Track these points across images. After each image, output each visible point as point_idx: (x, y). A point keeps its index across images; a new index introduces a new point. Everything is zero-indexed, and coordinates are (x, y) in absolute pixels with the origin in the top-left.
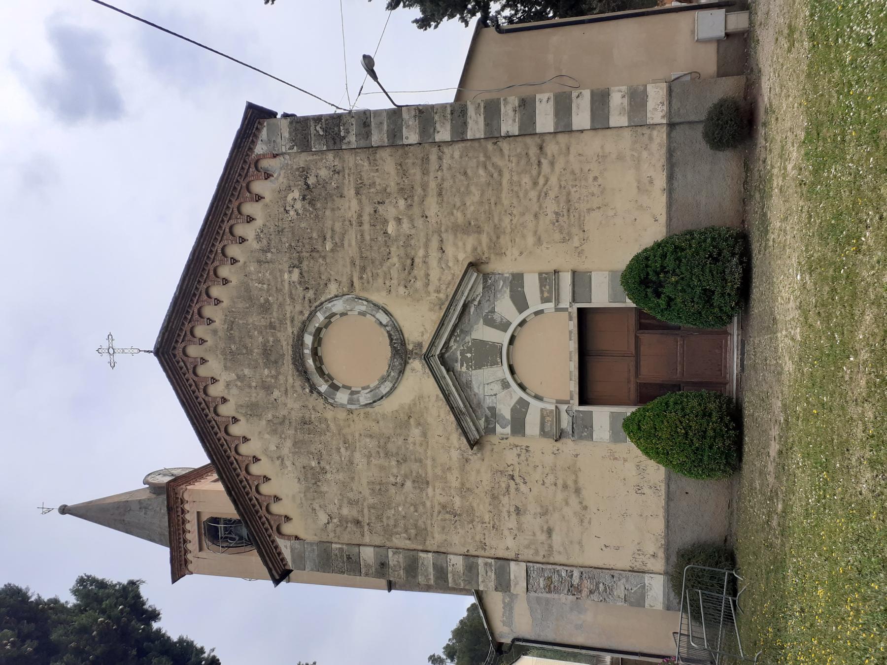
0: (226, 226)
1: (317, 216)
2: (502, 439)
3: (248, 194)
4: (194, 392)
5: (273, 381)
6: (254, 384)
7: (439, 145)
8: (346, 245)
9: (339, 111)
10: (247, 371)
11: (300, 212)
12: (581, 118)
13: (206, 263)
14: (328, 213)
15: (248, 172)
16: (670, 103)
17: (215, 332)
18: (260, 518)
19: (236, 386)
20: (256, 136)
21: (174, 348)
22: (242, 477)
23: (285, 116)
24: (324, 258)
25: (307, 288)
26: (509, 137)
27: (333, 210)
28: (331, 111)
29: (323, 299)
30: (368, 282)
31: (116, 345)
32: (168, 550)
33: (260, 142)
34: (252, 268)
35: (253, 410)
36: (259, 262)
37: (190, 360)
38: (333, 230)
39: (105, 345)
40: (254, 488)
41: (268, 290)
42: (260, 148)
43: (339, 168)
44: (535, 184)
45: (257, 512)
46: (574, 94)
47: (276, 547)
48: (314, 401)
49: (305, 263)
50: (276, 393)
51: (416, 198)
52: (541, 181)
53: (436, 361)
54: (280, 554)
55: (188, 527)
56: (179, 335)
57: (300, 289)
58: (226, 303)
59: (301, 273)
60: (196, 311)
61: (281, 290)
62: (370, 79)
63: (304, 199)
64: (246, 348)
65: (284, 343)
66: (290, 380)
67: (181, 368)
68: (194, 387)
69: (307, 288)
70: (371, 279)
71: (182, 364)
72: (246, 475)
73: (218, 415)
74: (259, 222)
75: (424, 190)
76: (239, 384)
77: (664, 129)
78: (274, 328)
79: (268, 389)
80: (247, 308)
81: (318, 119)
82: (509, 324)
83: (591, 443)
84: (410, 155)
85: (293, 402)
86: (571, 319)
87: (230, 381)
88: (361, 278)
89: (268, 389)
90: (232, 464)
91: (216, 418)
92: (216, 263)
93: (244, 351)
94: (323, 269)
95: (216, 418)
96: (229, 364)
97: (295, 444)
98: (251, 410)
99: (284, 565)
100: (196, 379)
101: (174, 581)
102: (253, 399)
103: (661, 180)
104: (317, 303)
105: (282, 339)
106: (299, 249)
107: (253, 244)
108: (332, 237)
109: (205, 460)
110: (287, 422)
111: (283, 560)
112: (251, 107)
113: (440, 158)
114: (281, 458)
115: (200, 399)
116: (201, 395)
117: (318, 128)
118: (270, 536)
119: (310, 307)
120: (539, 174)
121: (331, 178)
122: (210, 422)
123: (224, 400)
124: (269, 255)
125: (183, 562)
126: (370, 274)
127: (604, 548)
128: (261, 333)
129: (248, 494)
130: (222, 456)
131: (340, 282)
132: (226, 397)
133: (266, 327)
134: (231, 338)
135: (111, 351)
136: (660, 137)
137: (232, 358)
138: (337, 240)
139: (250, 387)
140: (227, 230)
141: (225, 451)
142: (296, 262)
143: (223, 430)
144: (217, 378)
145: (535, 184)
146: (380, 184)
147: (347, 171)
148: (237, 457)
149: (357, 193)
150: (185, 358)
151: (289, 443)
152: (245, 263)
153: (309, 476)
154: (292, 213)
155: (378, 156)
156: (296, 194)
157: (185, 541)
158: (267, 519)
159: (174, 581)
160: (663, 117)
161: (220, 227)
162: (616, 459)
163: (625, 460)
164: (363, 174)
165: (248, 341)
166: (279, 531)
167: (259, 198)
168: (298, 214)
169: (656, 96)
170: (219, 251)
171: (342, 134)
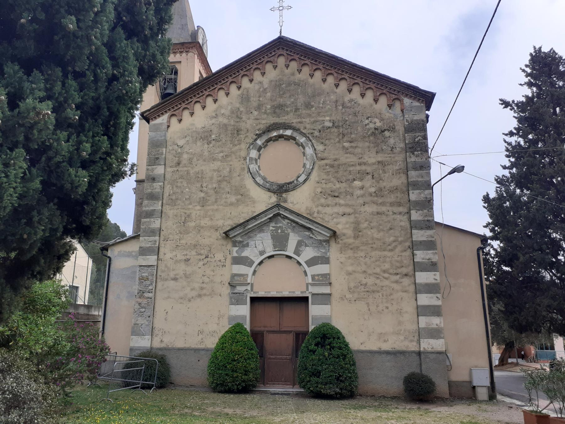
0: (358, 80)
1: (365, 137)
3: (378, 94)
4: (256, 62)
5: (263, 111)
6: (261, 99)
7: (409, 213)
8: (348, 155)
10: (269, 94)
11: (368, 127)
12: (425, 299)
13: (336, 68)
14: (367, 144)
17: (293, 74)
18: (180, 104)
19: (260, 88)
20: (415, 99)
21: (283, 49)
23: (427, 117)
24: (339, 142)
25: (320, 131)
27: (369, 147)
28: (430, 145)
29: (313, 141)
30: (324, 169)
31: (285, 11)
33: (411, 101)
34: (333, 97)
35: (245, 99)
36: (337, 101)
38: (356, 147)
40: (198, 100)
41: (319, 107)
42: (407, 101)
43: (394, 150)
44: (384, 272)
45: (184, 102)
46: (439, 295)
48: (251, 136)
49: (336, 130)
50: (256, 113)
51: (376, 198)
52: (386, 275)
54: (159, 116)
57: (320, 127)
59: (329, 127)
60: (306, 62)
63: (375, 129)
65: (286, 118)
66: (264, 122)
68: (259, 61)
69: (320, 131)
70: (326, 171)
71: (273, 54)
73: (242, 77)
74: (361, 101)
75: (381, 204)
76: (261, 90)
77: (417, 349)
81: (425, 138)
83: (228, 304)
85: (251, 123)
86: (302, 292)
87: (262, 84)
88: (326, 165)
89: (259, 107)
90: (213, 86)
92: (335, 74)
94: (332, 141)
96: (273, 83)
97: (225, 125)
102: (252, 99)
103: (386, 347)
104: (311, 138)
105: (289, 116)
108: (352, 147)
110: (238, 120)
113: (400, 213)
114: (216, 116)
115: (252, 66)
118: (169, 110)
120: (390, 274)
121: (388, 146)
123: (251, 81)
124: (341, 107)
126: (328, 170)
129: (195, 96)
130: (217, 79)
133: (296, 106)
134: (289, 84)
135: (281, 8)
136: (413, 347)
137: (277, 85)
139: (260, 97)
140: (356, 81)
142: (336, 124)
143: (233, 80)
144: (265, 76)
145: (384, 272)
147: (393, 155)
148: (217, 89)
149: (379, 162)
150: (277, 56)
151: (225, 121)
152: (336, 93)
154: (367, 122)
155: (402, 175)
156: (378, 124)
160: (424, 348)
161: (358, 77)
162: (219, 319)
163: (218, 324)
164: (391, 165)
165: (288, 95)
168: (366, 125)
169: (437, 344)
171: (416, 153)
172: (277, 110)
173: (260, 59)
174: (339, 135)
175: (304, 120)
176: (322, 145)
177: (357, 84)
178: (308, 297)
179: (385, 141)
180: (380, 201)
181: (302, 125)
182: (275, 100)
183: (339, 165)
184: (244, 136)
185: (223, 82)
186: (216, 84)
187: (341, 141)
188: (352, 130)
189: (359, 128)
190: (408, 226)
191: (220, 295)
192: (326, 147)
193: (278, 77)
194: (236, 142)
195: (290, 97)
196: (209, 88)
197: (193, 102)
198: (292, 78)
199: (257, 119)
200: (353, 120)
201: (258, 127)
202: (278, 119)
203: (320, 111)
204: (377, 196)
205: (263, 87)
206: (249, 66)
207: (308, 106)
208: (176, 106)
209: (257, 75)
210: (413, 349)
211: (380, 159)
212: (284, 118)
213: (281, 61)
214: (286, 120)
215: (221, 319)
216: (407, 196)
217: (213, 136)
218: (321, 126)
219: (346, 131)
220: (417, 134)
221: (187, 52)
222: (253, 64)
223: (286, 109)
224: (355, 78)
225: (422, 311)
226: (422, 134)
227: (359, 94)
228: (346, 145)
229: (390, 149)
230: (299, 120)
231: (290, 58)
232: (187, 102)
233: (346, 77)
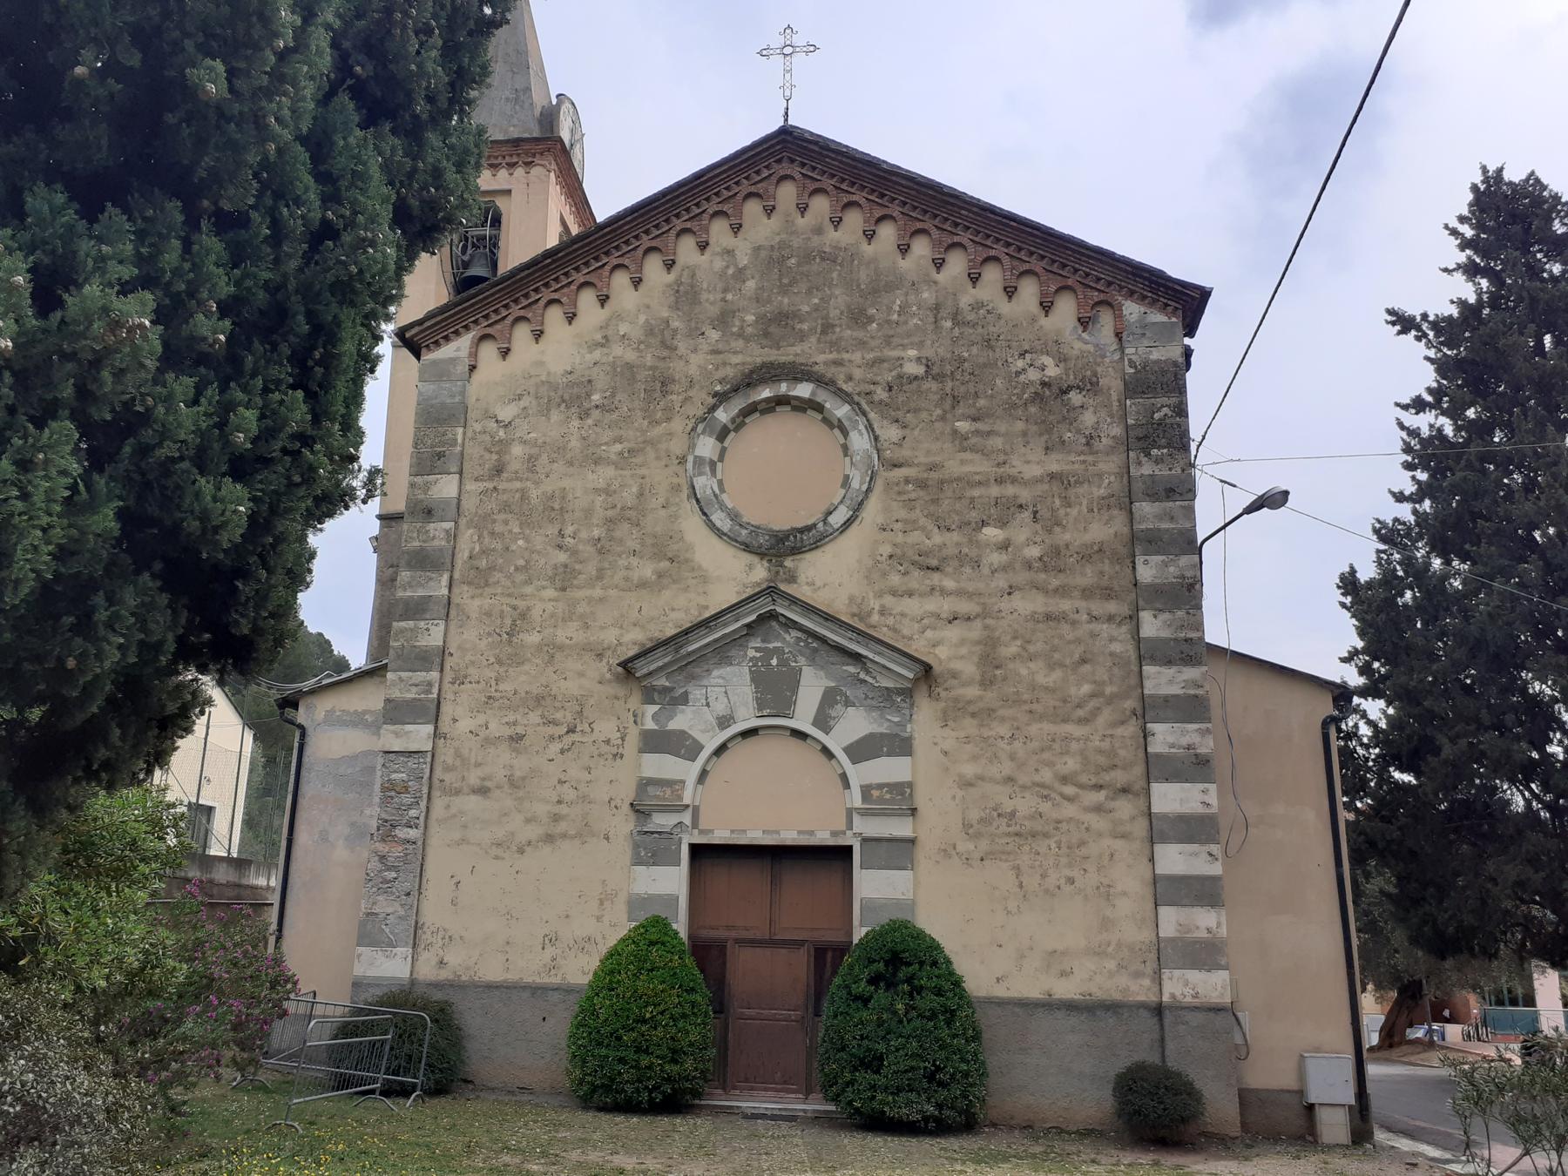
0: (999, 250)
1: (1014, 406)
3: (1053, 288)
4: (717, 194)
6: (729, 297)
7: (1134, 618)
8: (968, 456)
10: (751, 284)
11: (1022, 377)
12: (1175, 859)
13: (936, 216)
16: (1196, 1008)
17: (819, 231)
18: (506, 306)
23: (1188, 353)
25: (890, 389)
26: (1145, 737)
27: (1025, 434)
28: (1195, 432)
29: (872, 415)
30: (899, 493)
31: (799, 58)
33: (1143, 309)
35: (685, 295)
36: (937, 308)
38: (989, 433)
39: (799, 40)
41: (888, 322)
42: (1132, 310)
44: (1064, 780)
45: (516, 301)
46: (1214, 848)
49: (934, 386)
50: (714, 335)
52: (1069, 790)
59: (916, 378)
60: (854, 198)
63: (1044, 384)
65: (798, 349)
66: (736, 359)
68: (726, 194)
69: (890, 389)
70: (905, 497)
71: (765, 173)
73: (678, 235)
74: (1005, 307)
75: (1056, 590)
76: (730, 271)
77: (1154, 998)
78: (824, 332)
80: (859, 286)
81: (1181, 411)
84: (1117, 568)
85: (699, 362)
86: (834, 834)
88: (907, 481)
89: (723, 320)
90: (597, 259)
92: (935, 233)
93: (785, 281)
94: (924, 415)
96: (763, 254)
97: (629, 366)
102: (704, 296)
103: (1066, 989)
105: (805, 346)
107: (969, 295)
108: (977, 432)
110: (665, 353)
112: (1204, 295)
113: (1110, 618)
115: (705, 205)
120: (1081, 786)
121: (1078, 431)
122: (667, 221)
123: (703, 247)
124: (949, 324)
126: (913, 496)
127: (455, 880)
128: (816, 309)
130: (609, 242)
133: (826, 317)
134: (807, 257)
135: (788, 50)
136: (1140, 991)
137: (774, 259)
139: (725, 290)
140: (992, 253)
141: (617, 248)
143: (654, 244)
144: (740, 234)
145: (1064, 780)
147: (1090, 458)
148: (607, 268)
149: (1052, 476)
150: (774, 179)
151: (630, 356)
154: (1020, 364)
155: (1116, 512)
156: (1052, 371)
160: (1173, 996)
162: (602, 903)
163: (599, 919)
164: (1086, 486)
165: (803, 287)
168: (1018, 373)
169: (1210, 985)
170: (956, 239)
171: (1155, 452)
175: (846, 356)
177: (996, 259)
178: (850, 848)
179: (1070, 416)
182: (769, 301)
183: (942, 482)
186: (607, 253)
187: (949, 416)
191: (607, 839)
193: (777, 239)
198: (816, 240)
201: (720, 374)
203: (891, 332)
204: (1045, 569)
205: (736, 266)
207: (858, 318)
209: (719, 231)
211: (1055, 467)
212: (792, 350)
215: (607, 904)
216: (1129, 571)
219: (963, 389)
223: (798, 326)
227: (1000, 287)
228: (963, 426)
231: (812, 186)
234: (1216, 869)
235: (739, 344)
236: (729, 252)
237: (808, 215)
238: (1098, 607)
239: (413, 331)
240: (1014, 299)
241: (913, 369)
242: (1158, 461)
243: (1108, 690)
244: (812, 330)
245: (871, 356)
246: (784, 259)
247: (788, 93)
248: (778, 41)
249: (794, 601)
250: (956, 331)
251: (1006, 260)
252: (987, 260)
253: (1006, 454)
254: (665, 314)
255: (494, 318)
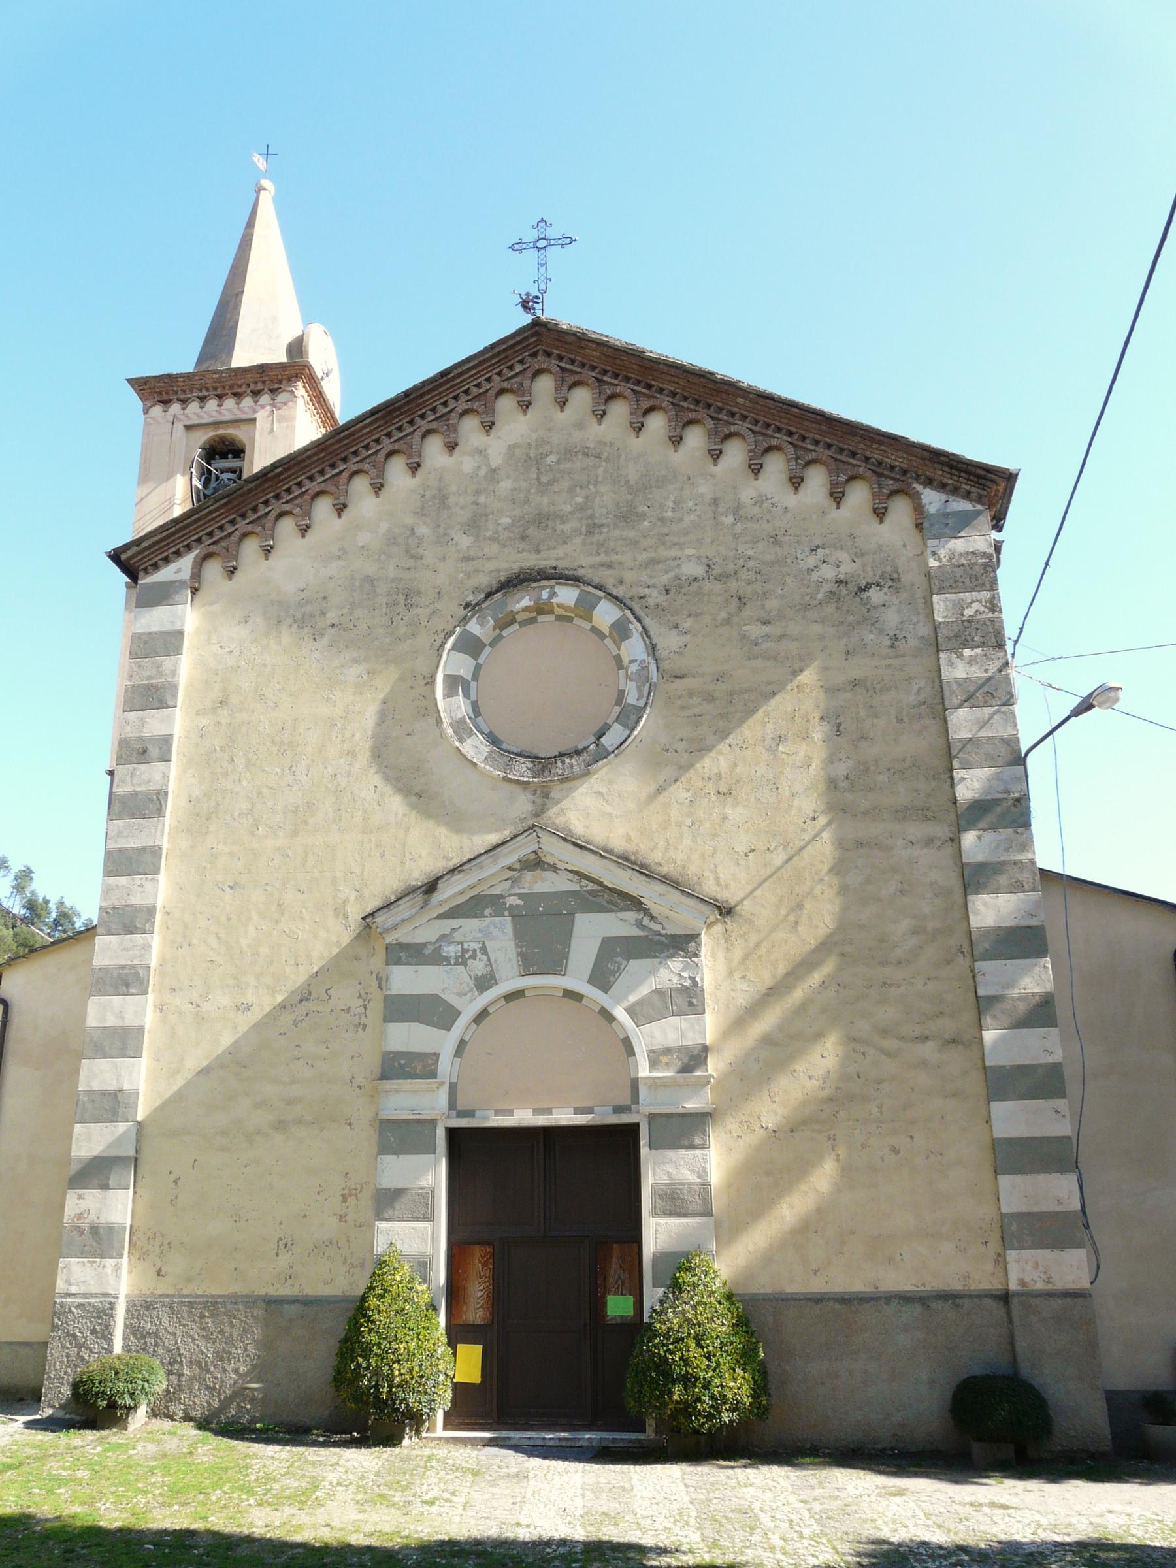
0: (779, 439)
1: (807, 607)
2: (379, 979)
3: (843, 478)
4: (466, 392)
5: (489, 534)
6: (482, 499)
7: (955, 840)
8: (759, 663)
9: (1009, 647)
10: (505, 485)
11: (815, 575)
12: (1013, 1119)
13: (709, 406)
14: (816, 628)
15: (887, 477)
16: (1050, 1295)
17: (580, 426)
18: (233, 522)
19: (479, 468)
20: (955, 491)
21: (548, 354)
22: (308, 485)
23: (998, 547)
24: (727, 622)
25: (667, 591)
26: (974, 977)
27: (822, 637)
28: (1010, 631)
29: (648, 621)
30: (683, 708)
31: (554, 252)
32: (191, 370)
33: (944, 497)
34: (704, 489)
35: (436, 502)
36: (715, 502)
37: (526, 383)
38: (782, 637)
39: (552, 233)
40: (287, 507)
41: (662, 520)
42: (932, 499)
43: (901, 644)
44: (884, 1032)
45: (243, 516)
46: (1061, 1103)
47: (178, 554)
48: (452, 608)
49: (718, 587)
50: (465, 541)
51: (850, 797)
52: (890, 1044)
53: (524, 848)
54: (167, 560)
55: (230, 403)
56: (573, 362)
57: (665, 579)
58: (636, 444)
59: (695, 579)
60: (618, 389)
61: (664, 544)
62: (1075, 702)
63: (840, 582)
64: (552, 482)
65: (560, 551)
66: (489, 566)
67: (511, 368)
68: (475, 391)
69: (667, 591)
70: (690, 712)
71: (518, 368)
72: (311, 492)
73: (424, 436)
74: (791, 500)
75: (866, 813)
76: (482, 472)
77: (996, 1285)
78: (589, 533)
79: (474, 525)
80: (627, 482)
81: (994, 606)
82: (605, 987)
83: (375, 1151)
84: (934, 784)
85: (451, 572)
86: (618, 1110)
87: (486, 457)
88: (691, 694)
89: (474, 525)
90: (333, 466)
91: (418, 434)
92: (710, 424)
93: (544, 479)
94: (707, 619)
95: (418, 434)
96: (519, 452)
97: (370, 580)
98: (434, 497)
99: (145, 570)
100: (492, 393)
101: (134, 382)
102: (452, 500)
103: (895, 1281)
104: (639, 612)
105: (568, 548)
106: (743, 574)
107: (748, 491)
108: (767, 636)
109: (343, 415)
110: (411, 563)
111: (156, 567)
112: (1009, 478)
113: (930, 841)
114: (343, 553)
115: (452, 404)
116: (462, 405)
117: (975, 606)
118: (199, 540)
119: (632, 599)
120: (901, 1038)
121: (881, 631)
122: (411, 422)
123: (452, 447)
124: (729, 520)
125: (165, 397)
126: (697, 711)
127: (173, 1177)
128: (581, 508)
129: (277, 497)
130: (348, 446)
131: (680, 654)
132: (457, 449)
133: (592, 517)
134: (569, 453)
135: (542, 244)
136: (984, 1280)
137: (532, 459)
138: (765, 646)
139: (477, 493)
140: (774, 442)
141: (356, 453)
142: (717, 570)
143: (396, 446)
144: (493, 432)
145: (884, 1032)
146: (873, 725)
147: (896, 662)
148: (345, 475)
149: (855, 684)
150: (529, 374)
151: (371, 569)
152: (712, 476)
153: (309, 609)
154: (811, 561)
155: (928, 721)
156: (847, 568)
157: (202, 399)
158: (230, 535)
159: (134, 382)
160: (1022, 1282)
161: (779, 430)
162: (344, 1198)
163: (342, 1218)
164: (893, 692)
165: (565, 484)
166: (207, 557)
167: (837, 497)
168: (810, 571)
169: (1069, 1268)
170: (733, 429)
171: (967, 652)
172: (532, 531)
173: (478, 386)
174: (727, 602)
175: (614, 558)
176: (674, 631)
177: (778, 448)
178: (637, 1125)
179: (870, 618)
180: (865, 804)
181: (610, 572)
182: (527, 501)
183: (731, 694)
184: (427, 611)
185: (364, 453)
186: (345, 460)
187: (735, 620)
188: (769, 586)
189: (789, 580)
190: (952, 880)
191: (350, 1124)
192: (687, 638)
193: (534, 436)
194: (403, 630)
195: (571, 490)
196: (322, 472)
197: (272, 516)
198: (578, 436)
199: (468, 559)
200: (769, 557)
201: (474, 582)
202: (534, 556)
203: (665, 531)
204: (852, 788)
205: (489, 465)
206: (445, 404)
207: (627, 516)
208: (221, 528)
209: (469, 428)
210: (985, 1286)
211: (857, 674)
212: (553, 553)
213: (545, 385)
214: (558, 559)
215: (351, 1201)
216: (947, 786)
217: (332, 616)
218: (672, 574)
219: (749, 589)
220: (968, 596)
221: (272, 391)
222: (456, 398)
223: (559, 527)
224: (769, 432)
225: (1019, 1156)
226: (988, 595)
227: (784, 477)
228: (755, 631)
229: (887, 642)
230: (602, 558)
231: (571, 379)
232: (252, 516)
233: (744, 431)
234: (1064, 1129)
235: (492, 549)
236: (481, 452)
237: (569, 408)
238: (916, 830)
239: (129, 553)
240: (802, 490)
241: (692, 569)
242: (971, 661)
243: (931, 925)
244: (577, 532)
245: (645, 556)
246: (543, 456)
247: (542, 287)
248: (531, 235)
249: (569, 839)
250: (738, 528)
251: (790, 450)
252: (768, 450)
253: (802, 660)
254: (409, 520)
255: (218, 535)
